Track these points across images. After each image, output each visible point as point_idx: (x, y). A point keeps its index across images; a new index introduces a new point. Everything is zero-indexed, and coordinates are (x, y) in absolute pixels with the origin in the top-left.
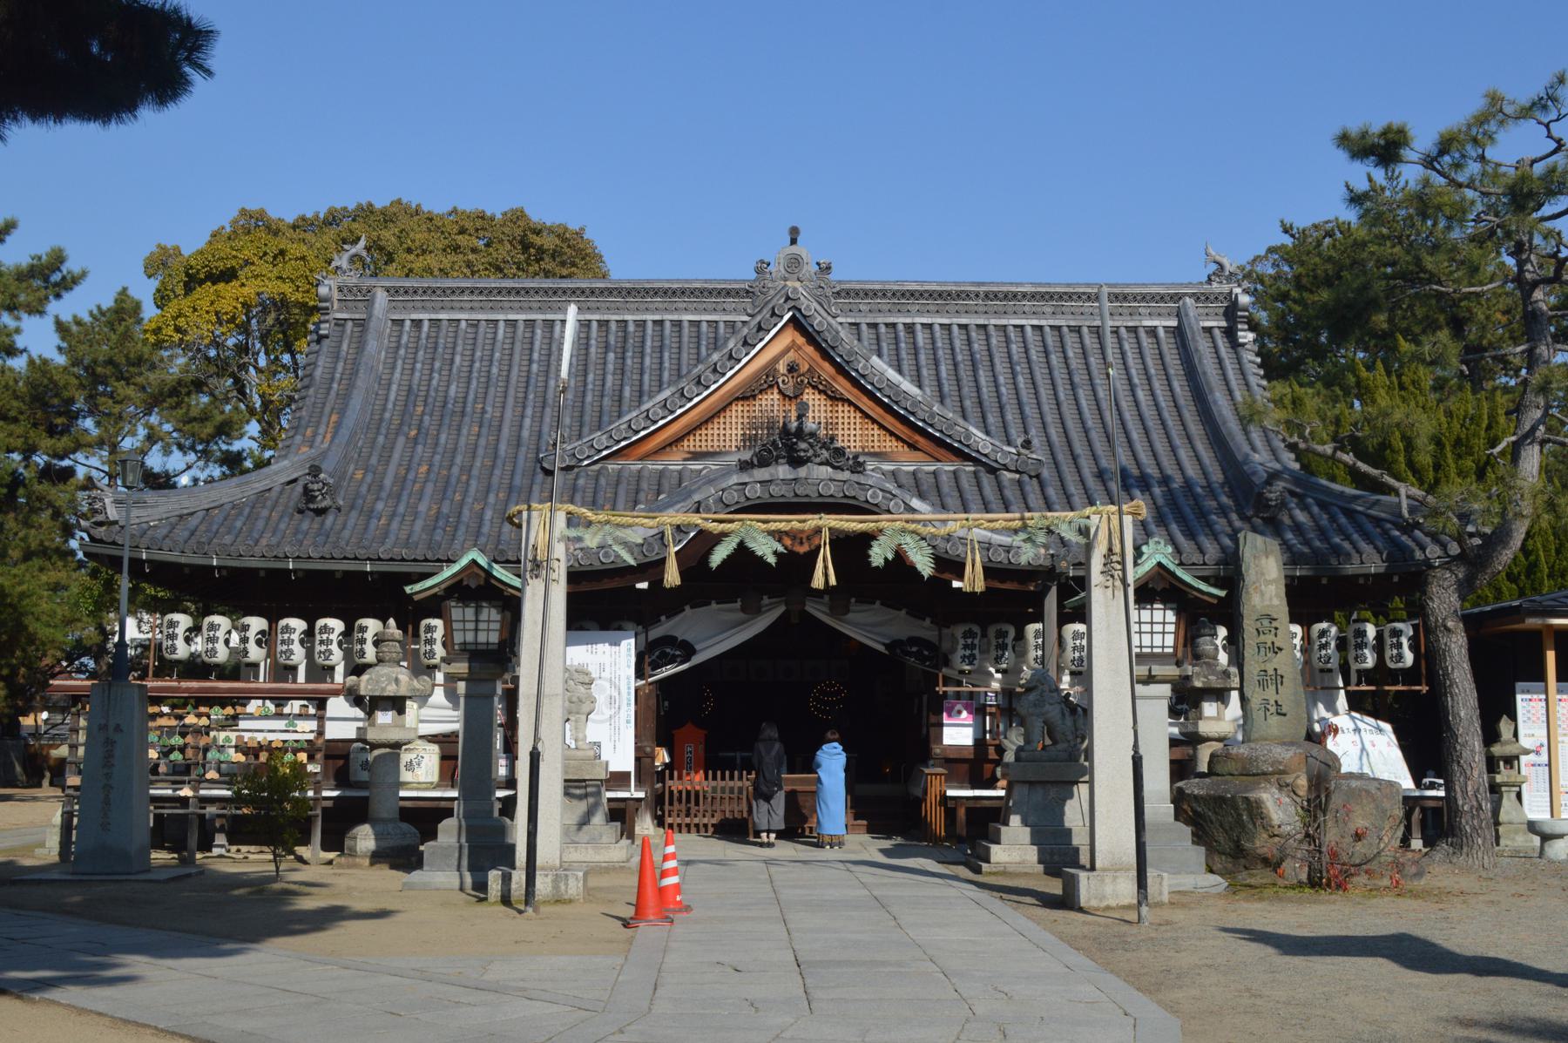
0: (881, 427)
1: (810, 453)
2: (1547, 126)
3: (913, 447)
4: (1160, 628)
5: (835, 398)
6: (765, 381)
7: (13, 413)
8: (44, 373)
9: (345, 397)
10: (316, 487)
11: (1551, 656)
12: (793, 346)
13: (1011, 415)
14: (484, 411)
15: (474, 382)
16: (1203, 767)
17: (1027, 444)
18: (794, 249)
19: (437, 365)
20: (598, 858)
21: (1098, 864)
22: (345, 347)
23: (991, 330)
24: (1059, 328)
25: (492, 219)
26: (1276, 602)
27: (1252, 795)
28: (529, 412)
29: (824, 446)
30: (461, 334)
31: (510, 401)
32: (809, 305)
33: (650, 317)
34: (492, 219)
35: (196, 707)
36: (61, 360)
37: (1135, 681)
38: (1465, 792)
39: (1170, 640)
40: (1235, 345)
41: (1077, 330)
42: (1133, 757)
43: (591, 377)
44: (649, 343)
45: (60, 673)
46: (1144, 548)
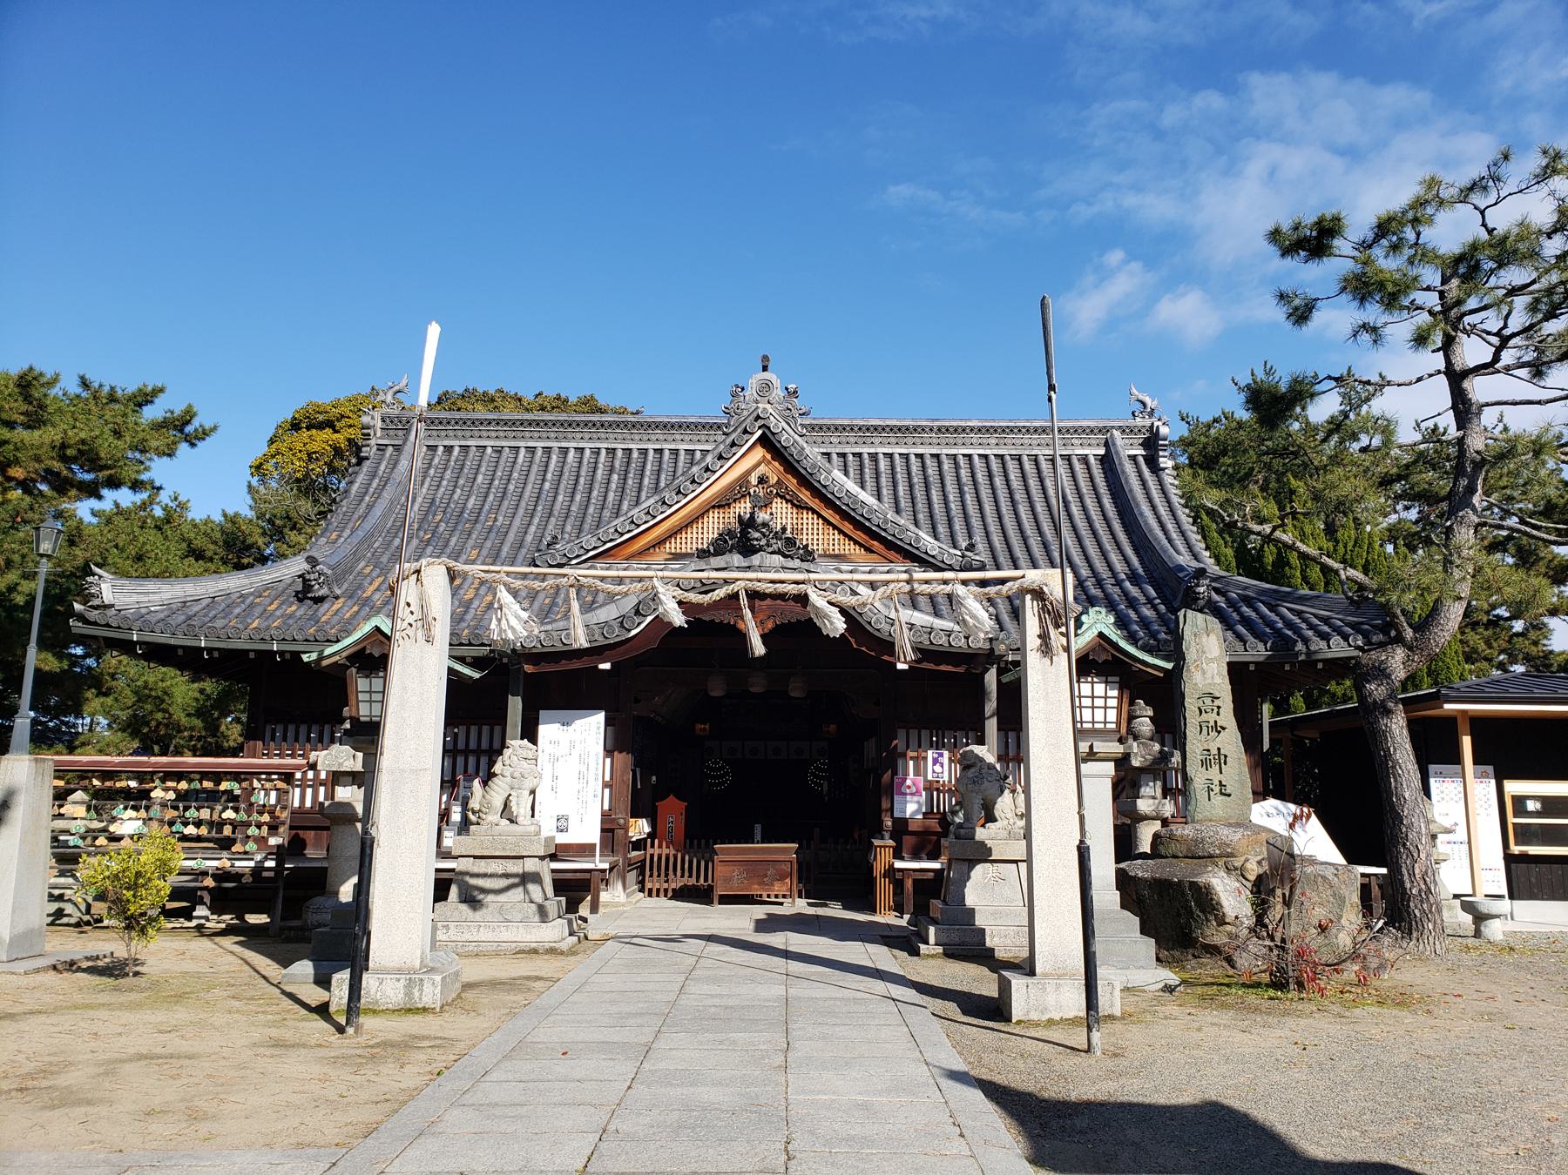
0: (841, 532)
1: (763, 542)
2: (1482, 213)
3: (868, 550)
4: (1103, 702)
5: (800, 506)
6: (739, 490)
7: (209, 554)
8: (234, 523)
9: (370, 507)
10: (312, 577)
11: (1467, 742)
12: (763, 461)
13: (958, 526)
14: (496, 520)
15: (491, 497)
16: (1145, 846)
17: (971, 547)
18: (766, 375)
19: (461, 482)
20: (529, 938)
21: (1038, 970)
22: (382, 467)
23: (944, 458)
24: (1002, 457)
25: (566, 400)
26: (1218, 680)
27: (1201, 880)
28: (536, 521)
29: (776, 536)
30: (486, 458)
31: (521, 511)
32: (777, 424)
33: (651, 446)
34: (566, 400)
35: (163, 780)
36: (251, 514)
37: (1080, 759)
38: (1412, 875)
39: (1112, 715)
40: (1155, 468)
41: (1019, 458)
42: (1079, 848)
43: (595, 493)
44: (649, 467)
45: (83, 744)
46: (1084, 618)
